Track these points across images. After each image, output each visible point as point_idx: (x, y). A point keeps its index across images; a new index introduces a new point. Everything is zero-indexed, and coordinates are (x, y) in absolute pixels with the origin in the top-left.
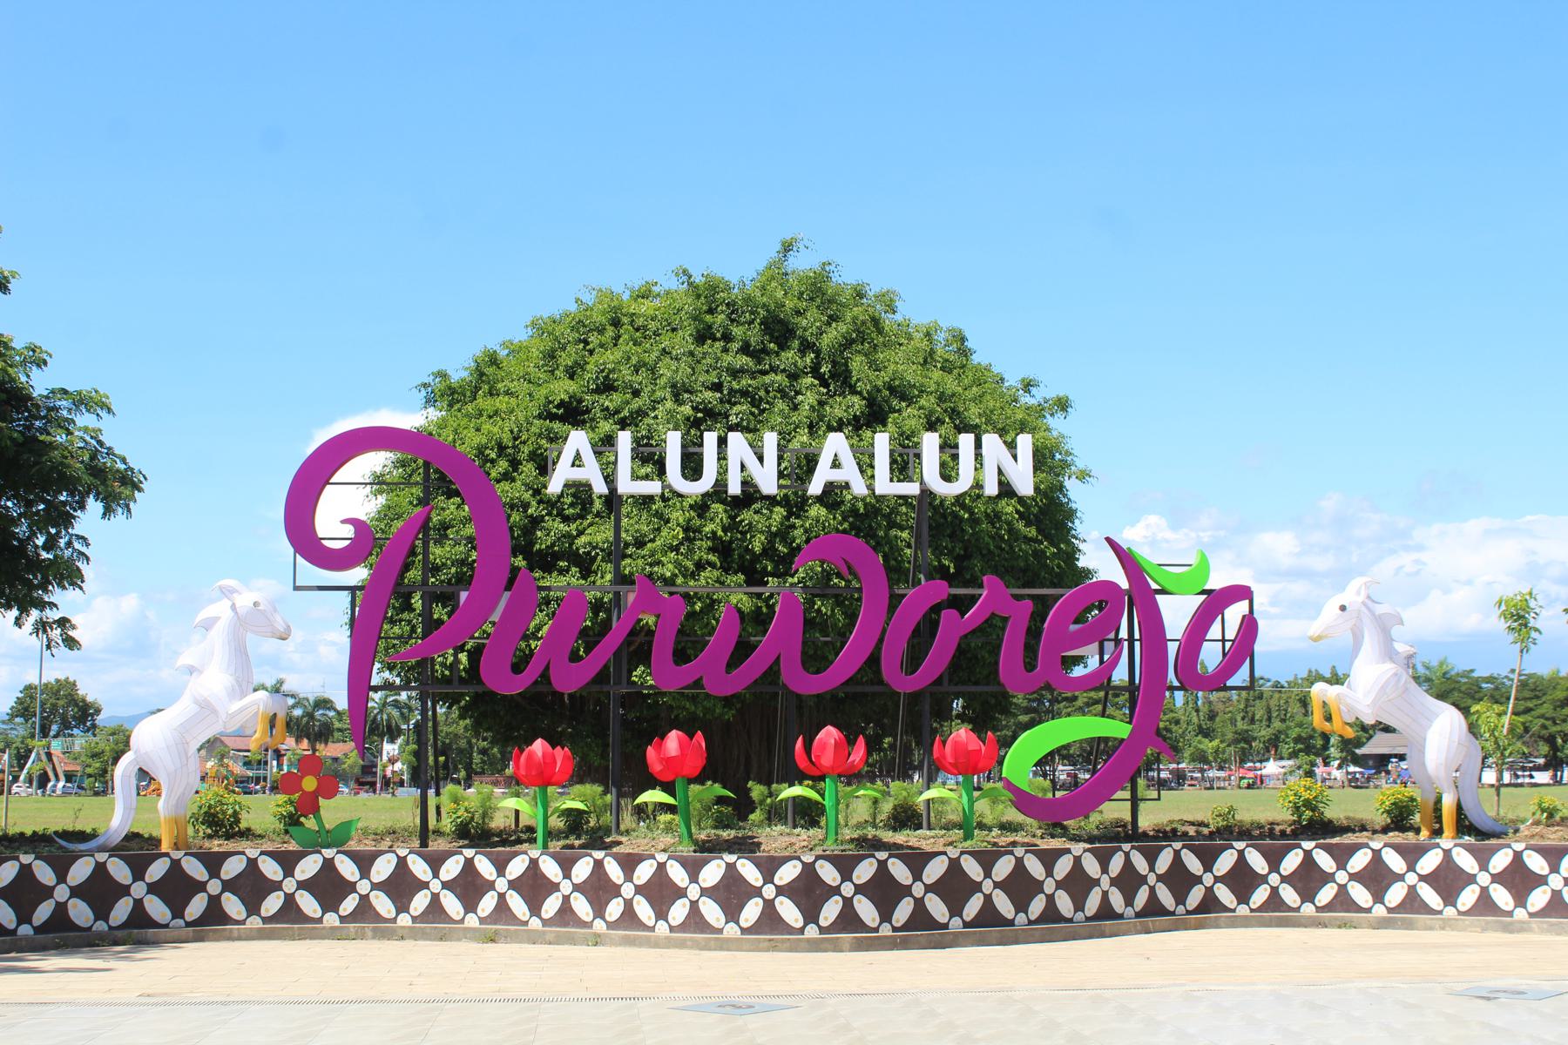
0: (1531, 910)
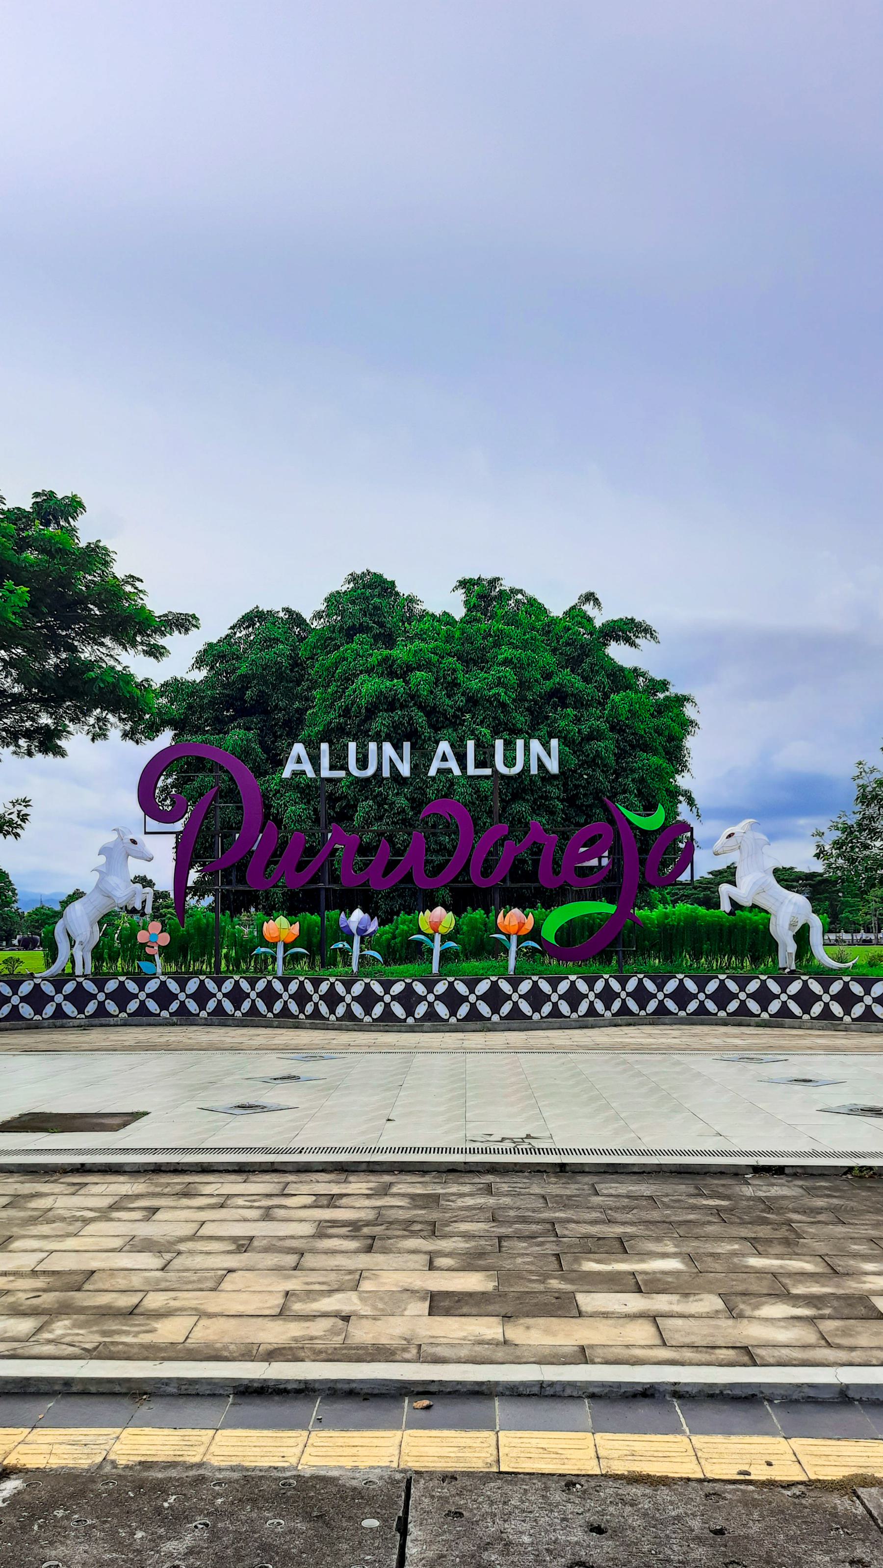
0: (854, 1016)
